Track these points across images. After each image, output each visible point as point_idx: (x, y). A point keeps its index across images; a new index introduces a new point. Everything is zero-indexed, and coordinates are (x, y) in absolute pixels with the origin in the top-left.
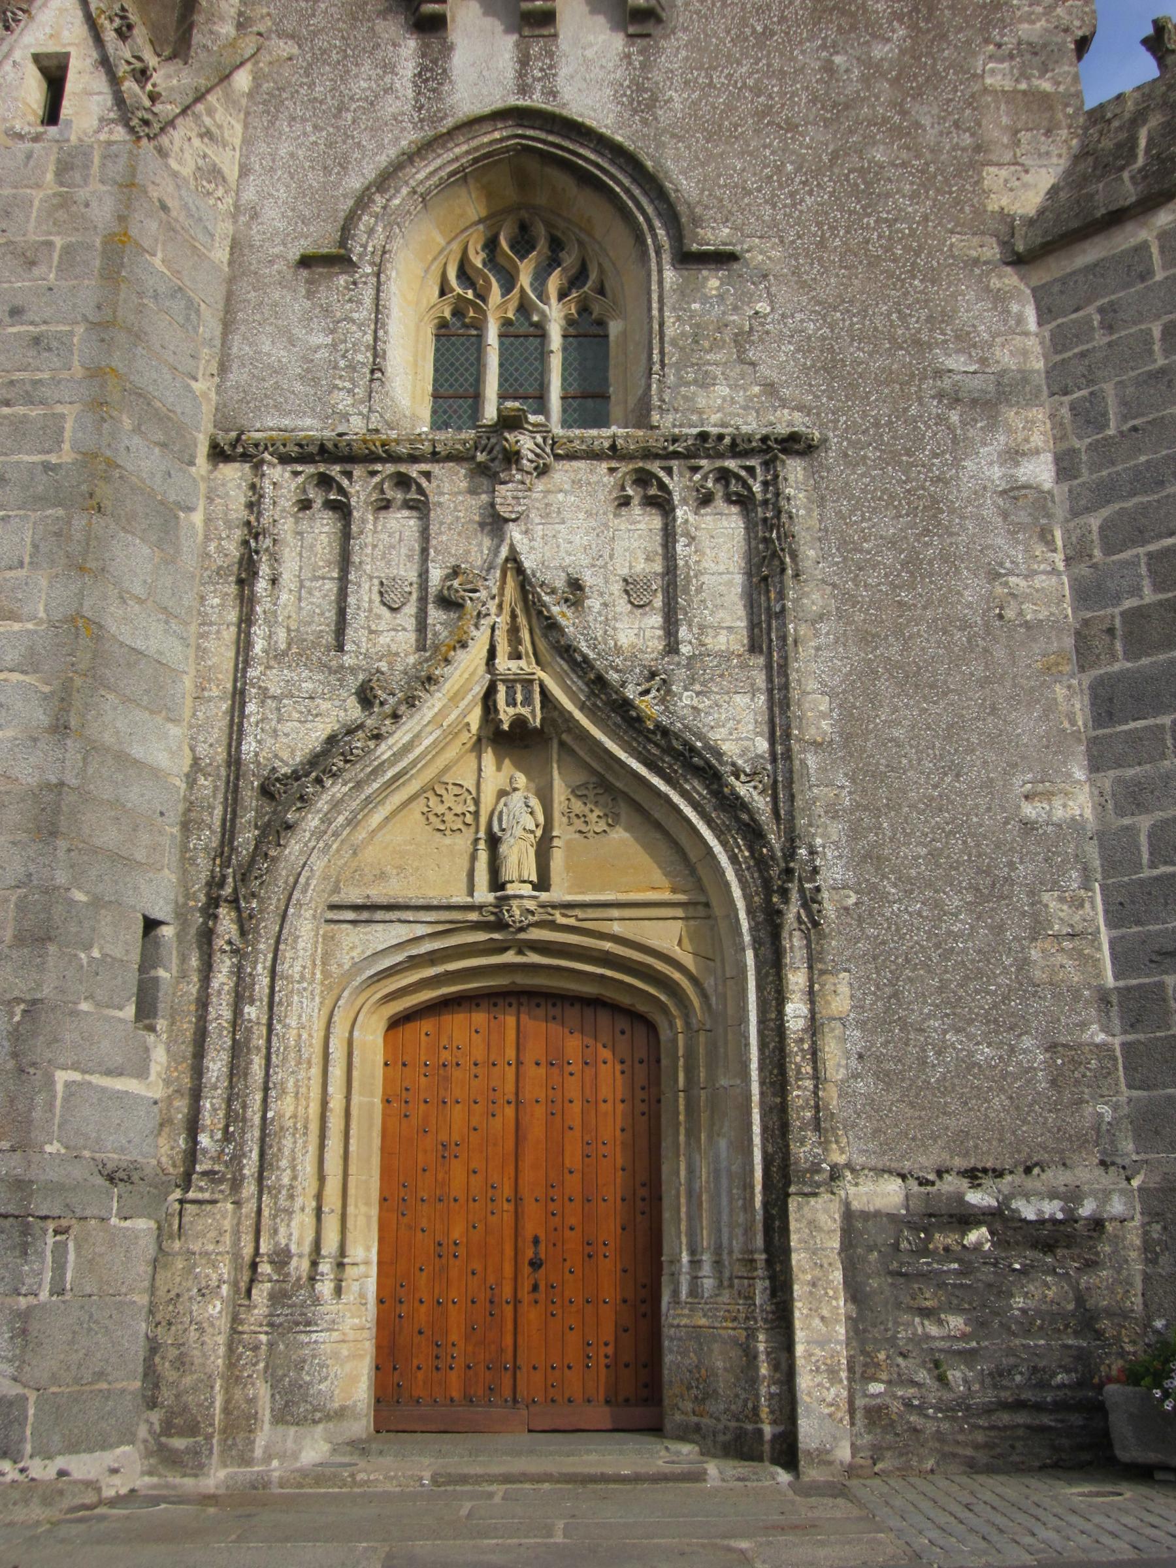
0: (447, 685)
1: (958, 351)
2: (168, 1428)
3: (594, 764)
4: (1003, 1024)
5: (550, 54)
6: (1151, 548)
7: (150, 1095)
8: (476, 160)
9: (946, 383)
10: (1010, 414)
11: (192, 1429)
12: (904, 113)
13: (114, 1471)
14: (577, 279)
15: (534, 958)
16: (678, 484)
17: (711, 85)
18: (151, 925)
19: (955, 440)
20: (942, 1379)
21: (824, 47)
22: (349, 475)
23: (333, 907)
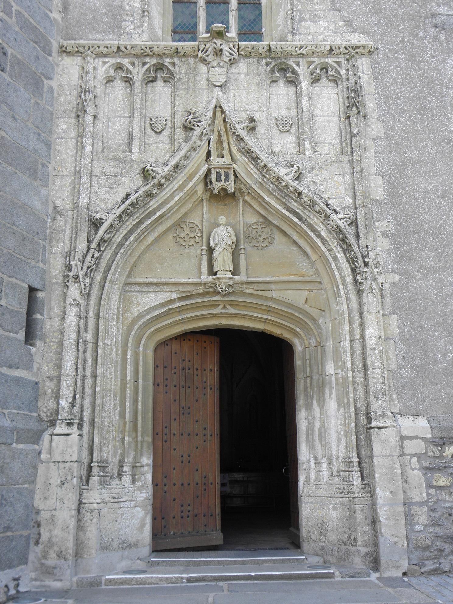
0: (186, 171)
3: (262, 212)
7: (34, 379)
9: (438, 21)
16: (302, 71)
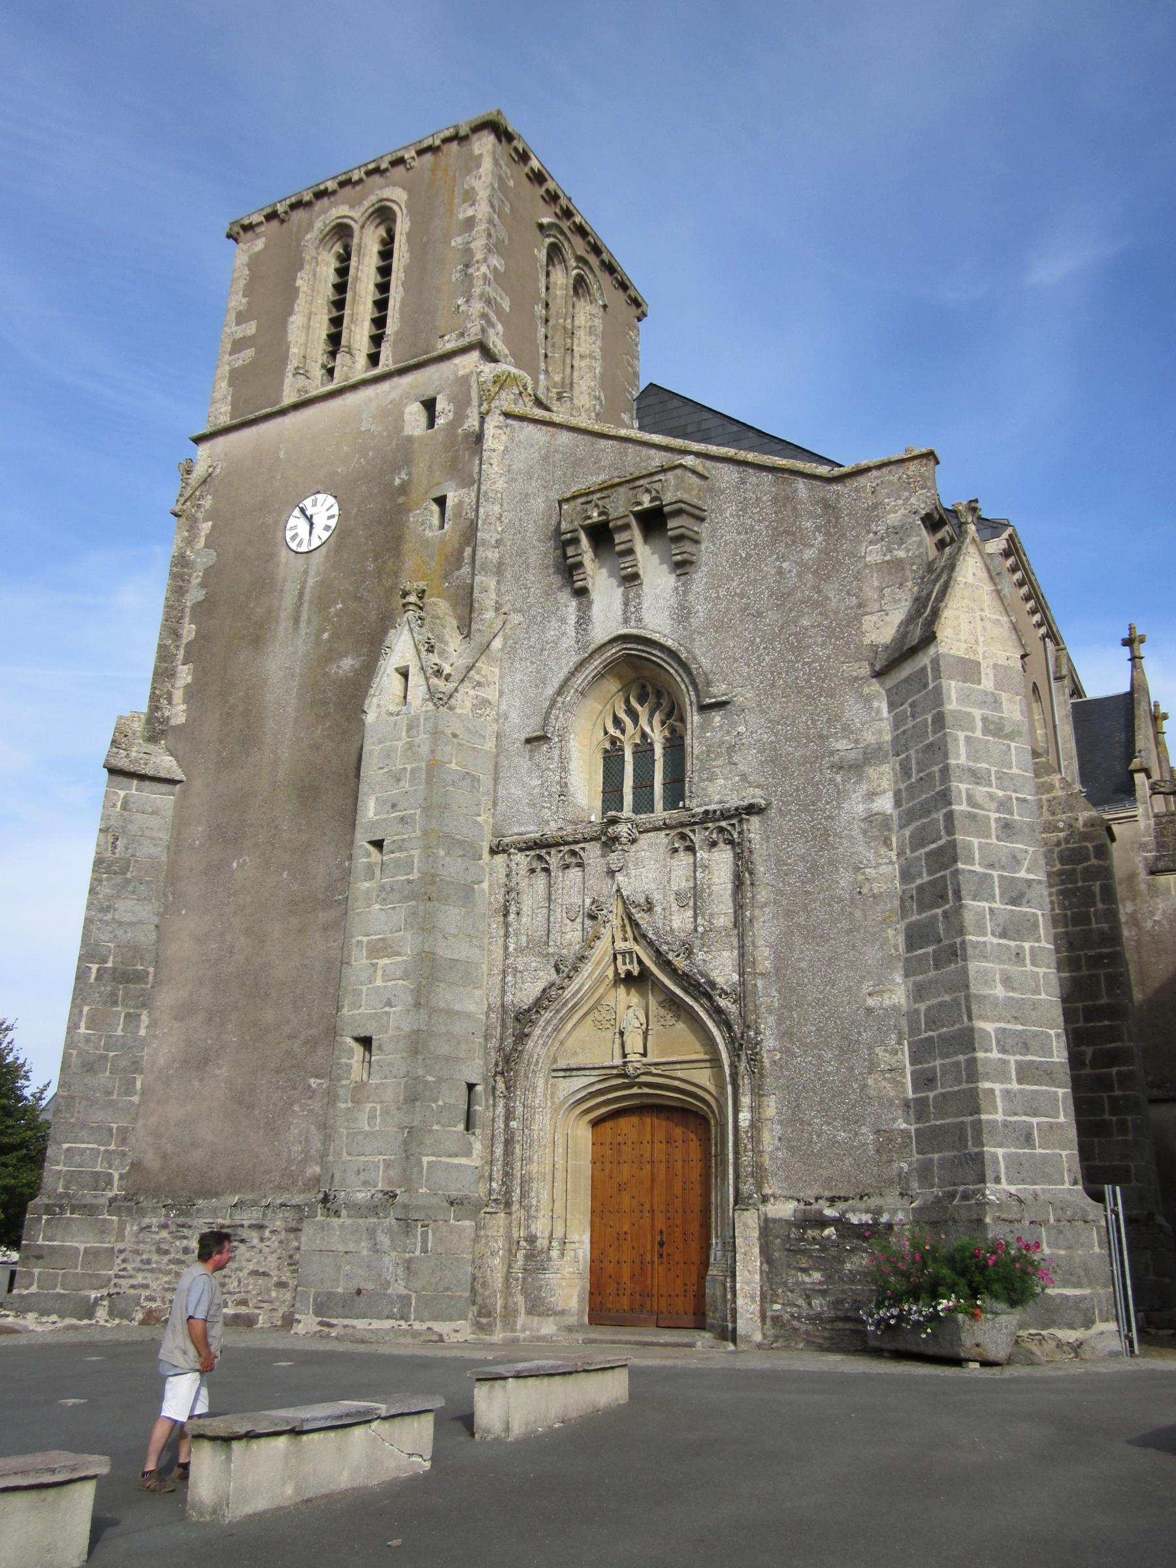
1: (842, 738)
2: (480, 1314)
4: (852, 1120)
5: (639, 596)
6: (927, 849)
8: (605, 667)
9: (836, 758)
10: (871, 771)
11: (489, 1315)
12: (819, 592)
13: (457, 1331)
14: (669, 715)
15: (646, 1090)
16: (697, 838)
17: (718, 597)
18: (471, 1087)
19: (839, 793)
20: (810, 1304)
21: (777, 559)
22: (549, 853)
23: (554, 1070)
